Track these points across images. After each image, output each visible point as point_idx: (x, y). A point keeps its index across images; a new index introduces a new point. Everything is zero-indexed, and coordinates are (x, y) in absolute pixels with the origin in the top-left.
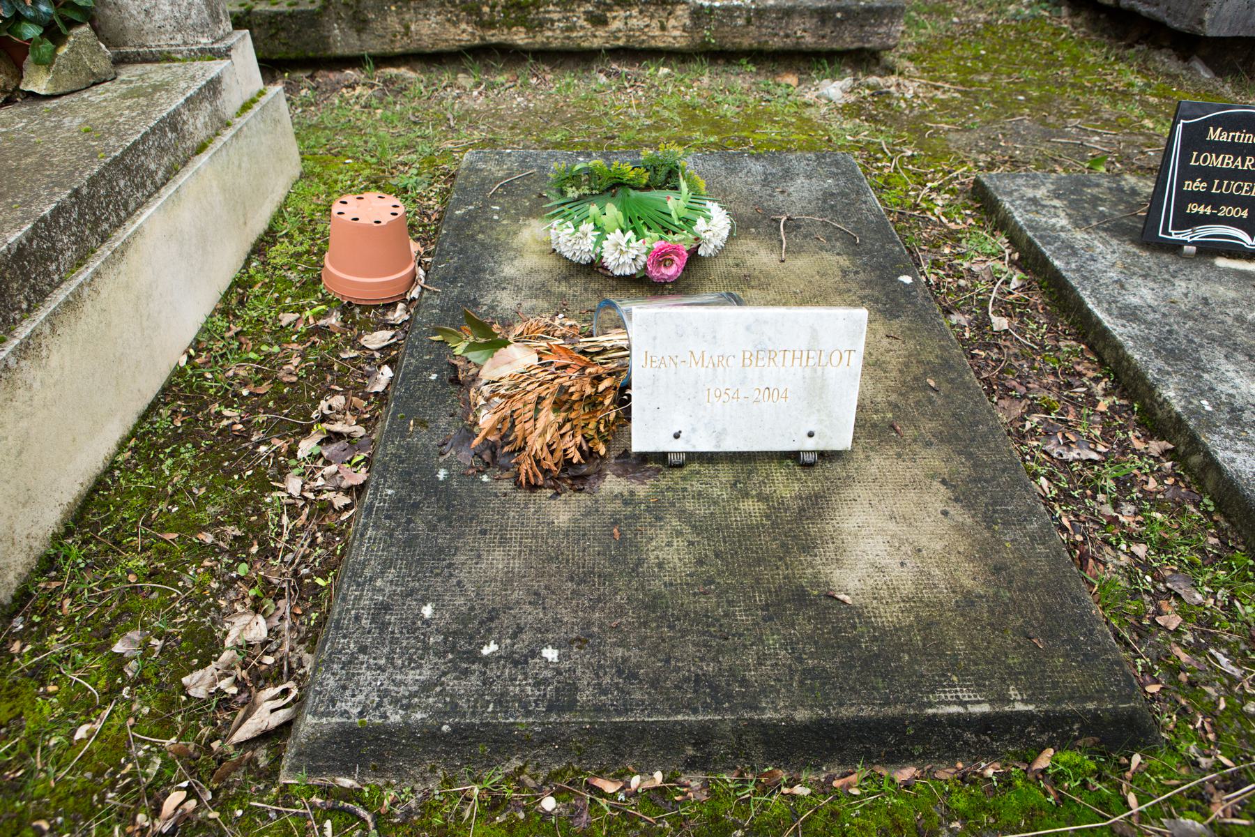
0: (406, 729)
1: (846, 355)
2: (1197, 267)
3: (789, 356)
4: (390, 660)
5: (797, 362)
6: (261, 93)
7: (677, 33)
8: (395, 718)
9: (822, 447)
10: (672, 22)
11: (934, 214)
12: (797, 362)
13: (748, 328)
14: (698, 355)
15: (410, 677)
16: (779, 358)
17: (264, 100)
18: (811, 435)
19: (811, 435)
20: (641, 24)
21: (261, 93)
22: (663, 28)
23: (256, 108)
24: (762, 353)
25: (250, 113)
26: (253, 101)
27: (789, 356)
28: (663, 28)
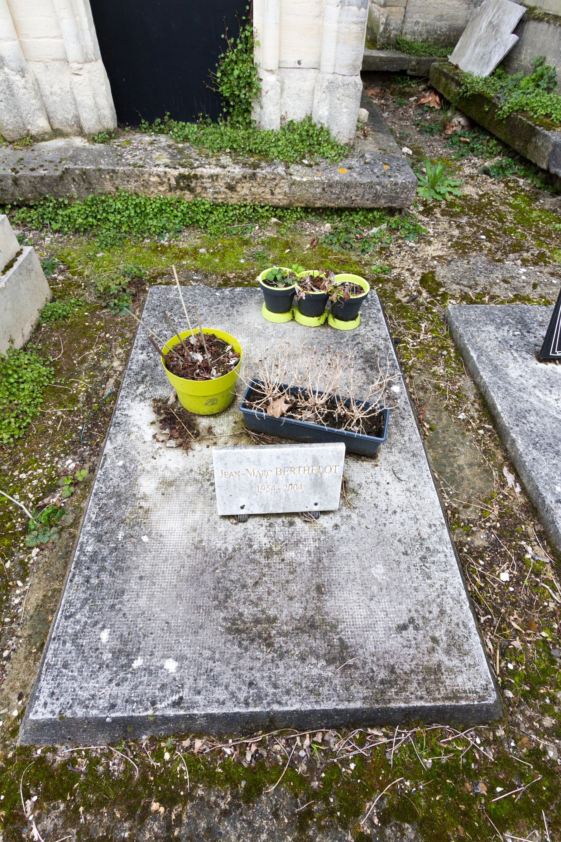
0: (87, 720)
1: (334, 468)
2: (524, 466)
3: (302, 469)
4: (80, 672)
5: (306, 472)
6: (19, 253)
7: (281, 197)
8: (80, 712)
9: (322, 509)
10: (278, 190)
11: (232, 755)
12: (306, 472)
13: (278, 458)
14: (251, 471)
15: (91, 684)
16: (297, 470)
17: (20, 259)
18: (316, 504)
19: (316, 504)
20: (260, 191)
21: (19, 253)
22: (272, 194)
23: (16, 265)
24: (287, 468)
25: (12, 271)
26: (14, 260)
27: (302, 469)
28: (272, 194)
